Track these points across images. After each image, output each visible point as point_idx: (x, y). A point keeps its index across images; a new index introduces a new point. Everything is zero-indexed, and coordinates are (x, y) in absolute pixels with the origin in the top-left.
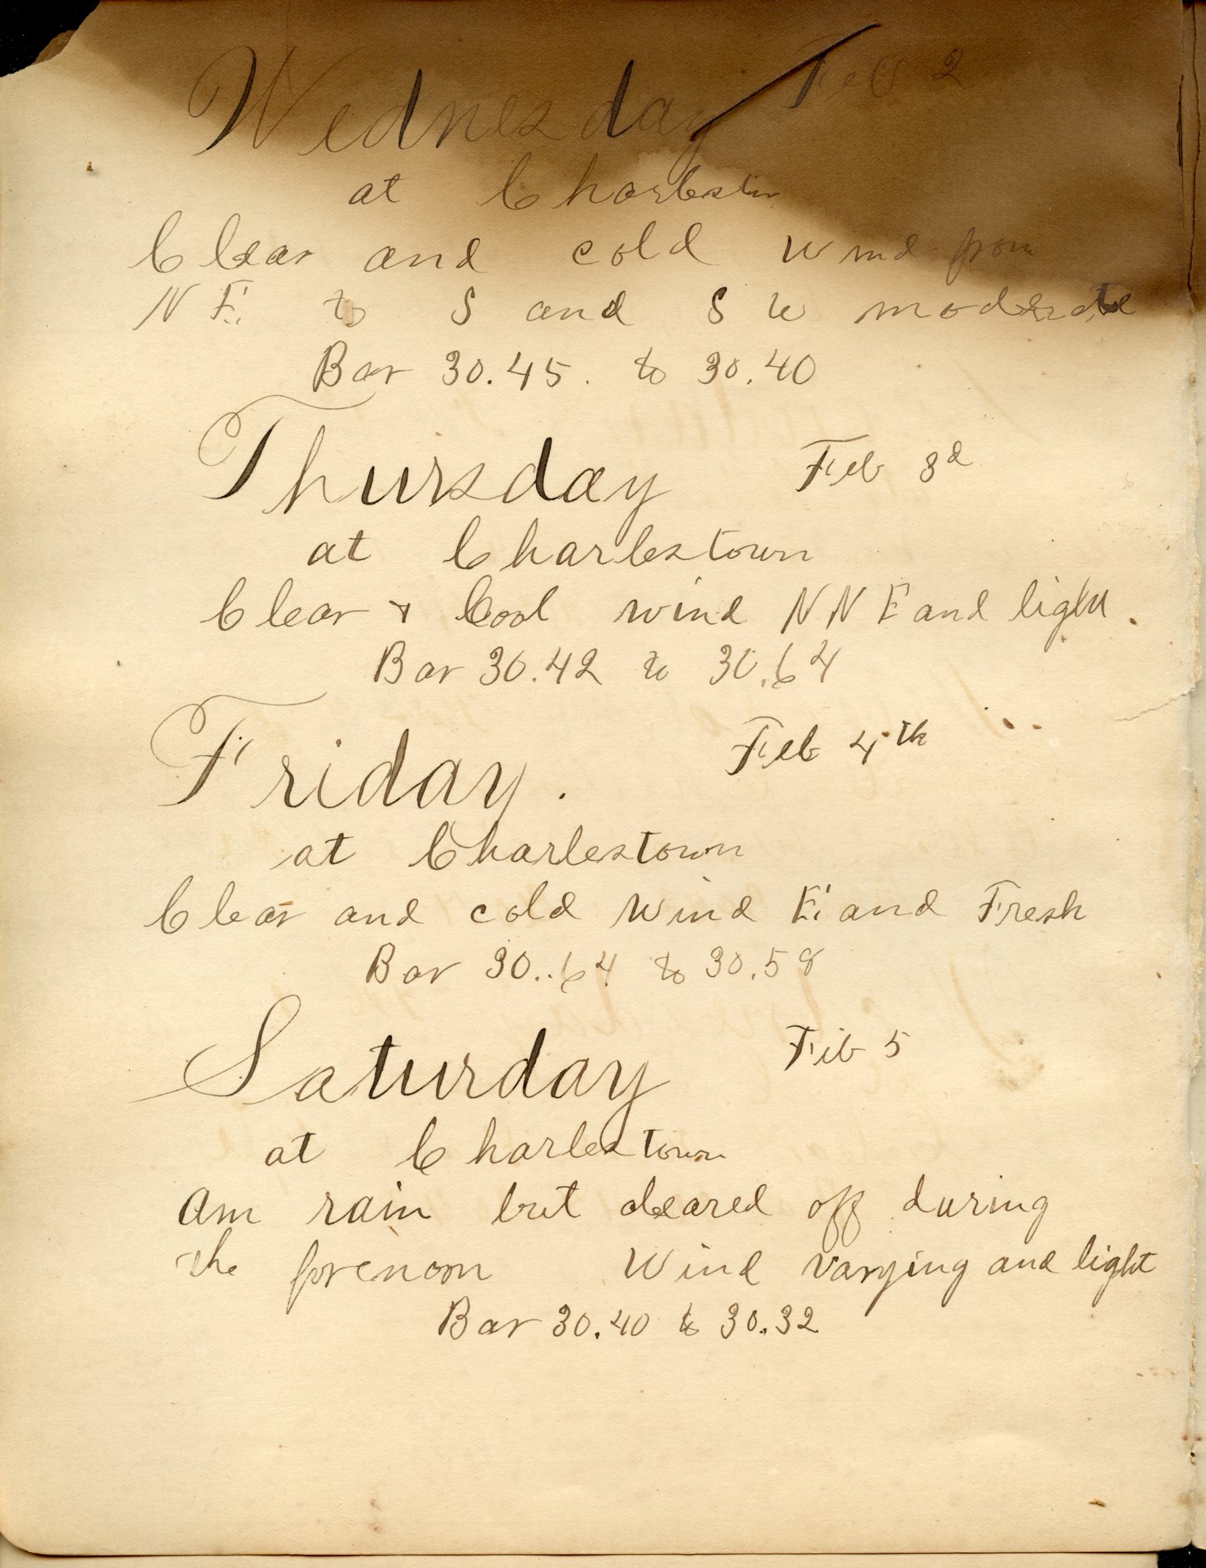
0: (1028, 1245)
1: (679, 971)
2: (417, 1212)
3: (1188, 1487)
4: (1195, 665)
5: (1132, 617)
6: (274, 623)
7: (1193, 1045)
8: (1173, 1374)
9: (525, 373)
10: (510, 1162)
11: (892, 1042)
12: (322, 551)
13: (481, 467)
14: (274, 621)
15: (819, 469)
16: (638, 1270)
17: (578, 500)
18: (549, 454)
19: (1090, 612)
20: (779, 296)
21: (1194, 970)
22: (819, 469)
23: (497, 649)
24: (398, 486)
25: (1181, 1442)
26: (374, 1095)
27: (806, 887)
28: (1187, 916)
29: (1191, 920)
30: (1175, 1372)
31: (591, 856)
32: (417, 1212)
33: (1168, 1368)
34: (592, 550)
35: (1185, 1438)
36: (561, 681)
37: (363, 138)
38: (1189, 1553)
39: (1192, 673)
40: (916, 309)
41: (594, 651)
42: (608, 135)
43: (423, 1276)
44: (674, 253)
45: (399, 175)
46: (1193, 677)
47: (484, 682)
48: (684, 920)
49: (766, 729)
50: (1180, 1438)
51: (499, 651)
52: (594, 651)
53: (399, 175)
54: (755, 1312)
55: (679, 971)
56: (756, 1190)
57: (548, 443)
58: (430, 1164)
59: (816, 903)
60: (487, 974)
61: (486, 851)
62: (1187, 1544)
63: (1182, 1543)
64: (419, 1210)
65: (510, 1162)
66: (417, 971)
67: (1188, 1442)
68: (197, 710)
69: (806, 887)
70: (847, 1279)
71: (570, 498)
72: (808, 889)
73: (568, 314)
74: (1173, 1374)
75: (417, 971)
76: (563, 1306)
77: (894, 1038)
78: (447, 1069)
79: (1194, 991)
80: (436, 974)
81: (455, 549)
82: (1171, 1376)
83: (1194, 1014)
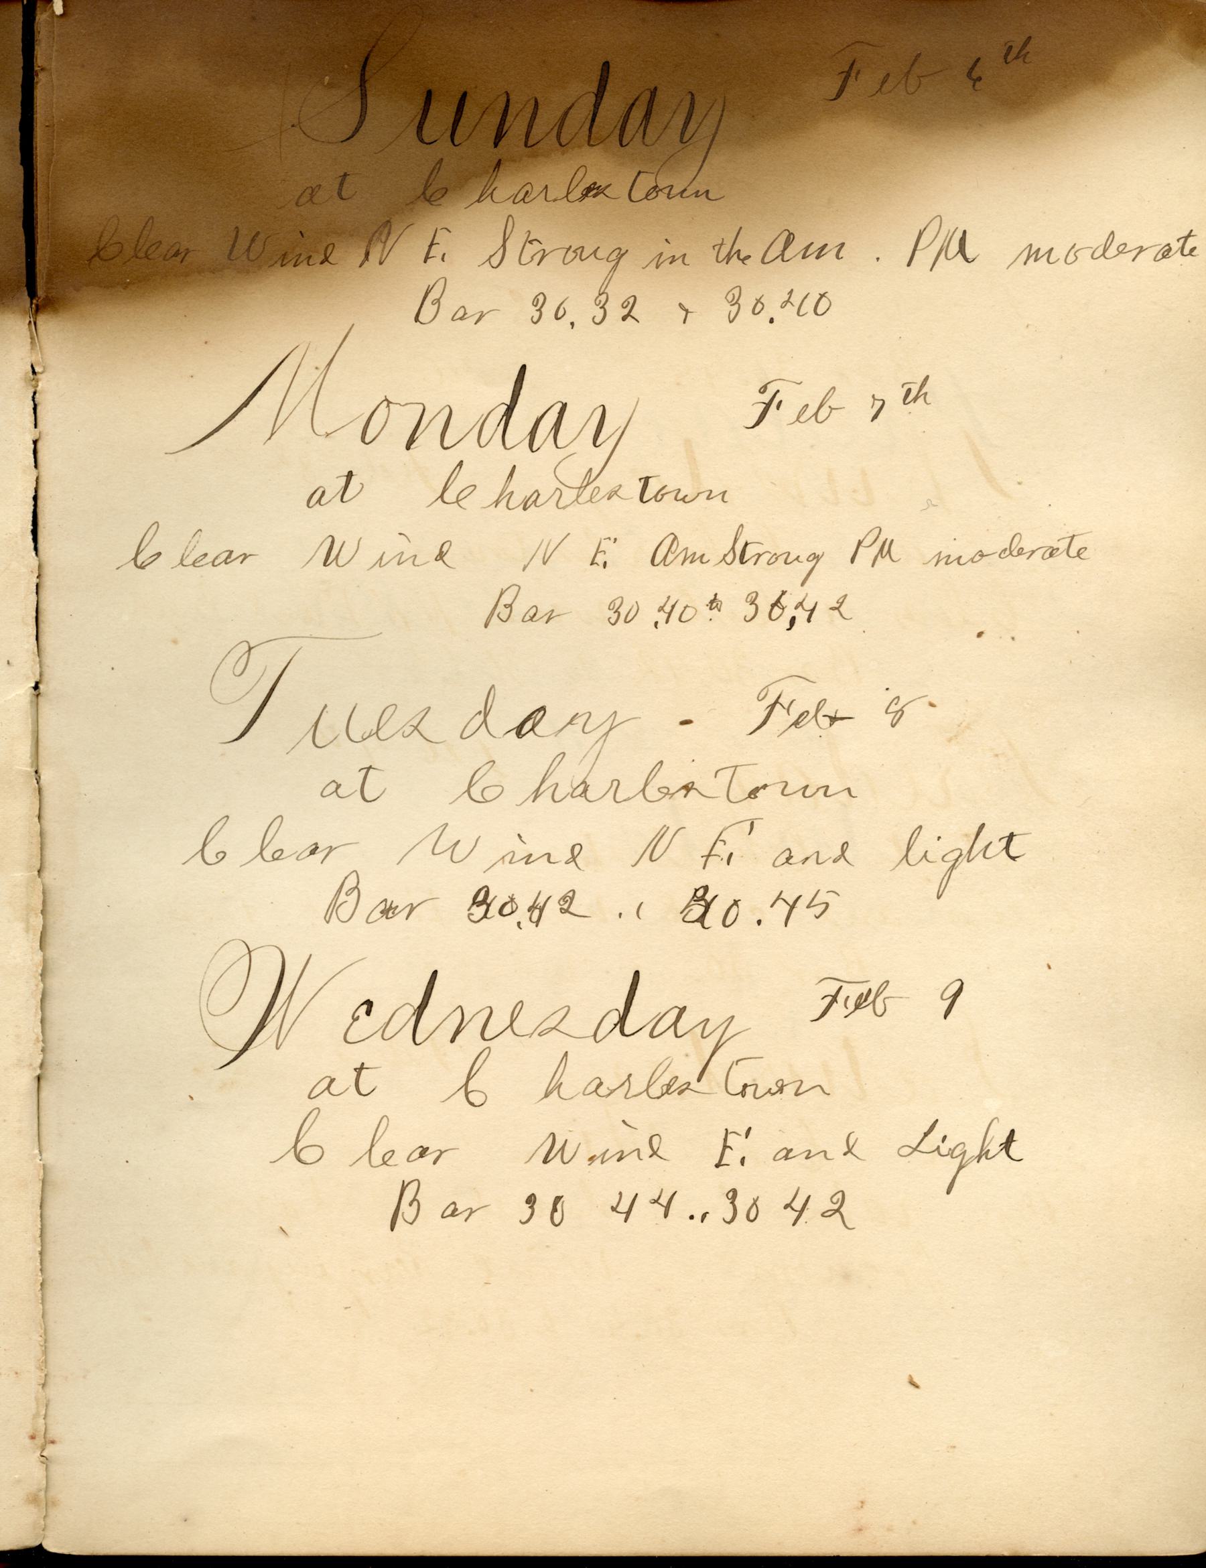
1: (363, 1064)
3: (36, 1487)
4: (33, 663)
6: (446, 499)
7: (35, 1044)
8: (17, 1373)
14: (446, 498)
15: (835, 1003)
21: (35, 970)
22: (835, 1003)
24: (414, 1018)
25: (28, 1441)
28: (27, 915)
29: (31, 920)
30: (19, 1371)
33: (11, 1368)
34: (555, 492)
35: (33, 1437)
36: (812, 619)
39: (30, 672)
46: (31, 675)
50: (27, 1437)
54: (630, 1075)
55: (363, 1064)
56: (762, 424)
61: (503, 498)
62: (37, 1543)
63: (31, 1542)
67: (36, 1441)
68: (412, 732)
74: (17, 1373)
79: (35, 991)
82: (15, 1376)
83: (35, 1013)
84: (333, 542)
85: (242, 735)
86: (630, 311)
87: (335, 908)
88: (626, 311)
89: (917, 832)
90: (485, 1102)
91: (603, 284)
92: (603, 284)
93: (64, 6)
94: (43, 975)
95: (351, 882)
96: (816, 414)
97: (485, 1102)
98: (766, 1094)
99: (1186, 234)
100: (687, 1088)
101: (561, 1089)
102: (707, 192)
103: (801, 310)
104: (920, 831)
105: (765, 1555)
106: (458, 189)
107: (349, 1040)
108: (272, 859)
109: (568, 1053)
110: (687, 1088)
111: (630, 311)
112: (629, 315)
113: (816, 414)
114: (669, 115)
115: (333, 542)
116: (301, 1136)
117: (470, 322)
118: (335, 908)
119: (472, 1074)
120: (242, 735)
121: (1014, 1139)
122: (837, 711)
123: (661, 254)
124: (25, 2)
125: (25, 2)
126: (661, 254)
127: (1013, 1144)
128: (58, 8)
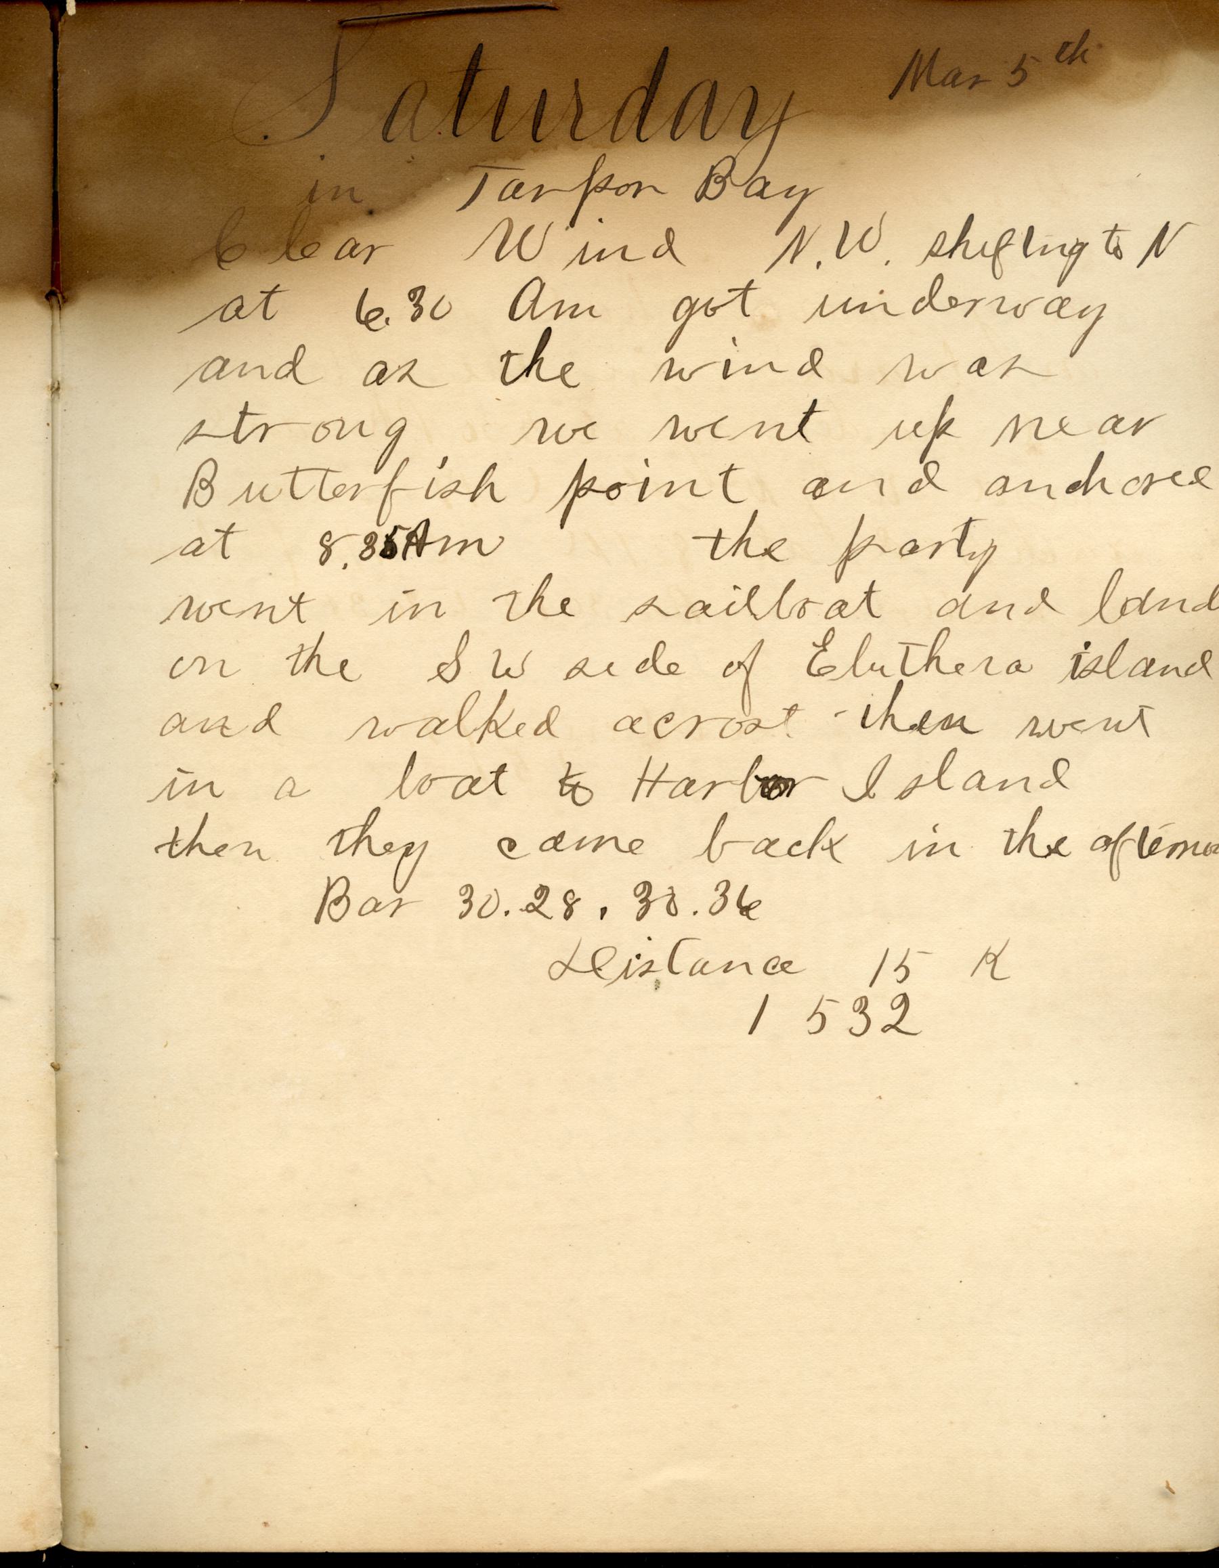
0: (1131, 678)
10: (581, 263)
11: (901, 966)
16: (457, 776)
17: (521, 319)
18: (546, 343)
19: (441, 497)
20: (993, 660)
26: (430, 496)
27: (809, 857)
37: (202, 371)
38: (646, 1559)
42: (235, 441)
45: (796, 705)
48: (434, 496)
53: (796, 705)
57: (1031, 230)
59: (934, 824)
65: (581, 263)
69: (809, 857)
71: (264, 427)
72: (806, 854)
77: (903, 962)
84: (1026, 246)
87: (442, 492)
90: (588, 802)
96: (861, 242)
97: (588, 802)
99: (727, 468)
100: (454, 490)
101: (745, 671)
103: (248, 846)
107: (749, 553)
108: (667, 672)
109: (966, 719)
110: (454, 490)
113: (861, 242)
114: (733, 102)
115: (1026, 246)
116: (657, 656)
117: (922, 556)
118: (442, 492)
121: (505, 770)
123: (245, 364)
126: (245, 364)
127: (807, 410)
128: (71, 8)
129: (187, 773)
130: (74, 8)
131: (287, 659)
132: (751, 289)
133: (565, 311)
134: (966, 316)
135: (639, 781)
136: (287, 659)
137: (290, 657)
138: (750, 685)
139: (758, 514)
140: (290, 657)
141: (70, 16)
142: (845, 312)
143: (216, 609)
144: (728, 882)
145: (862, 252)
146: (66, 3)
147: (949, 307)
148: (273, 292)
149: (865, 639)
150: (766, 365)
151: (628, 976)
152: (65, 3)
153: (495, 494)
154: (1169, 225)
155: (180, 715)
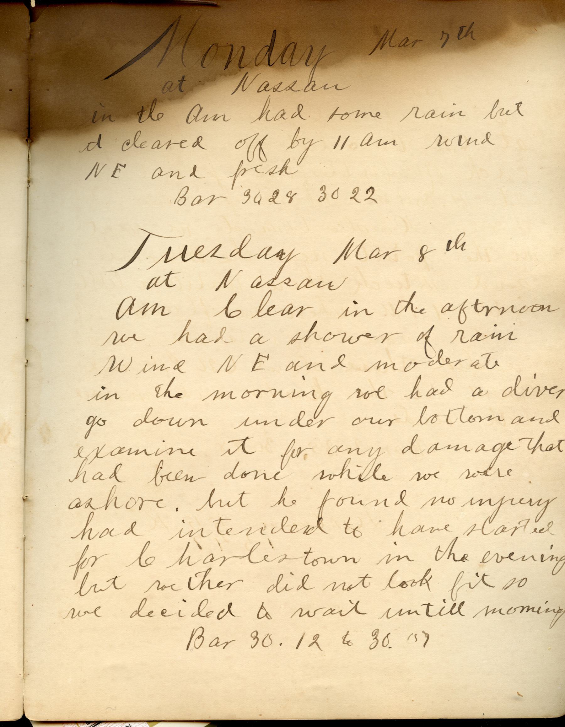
2: (144, 452)
5: (94, 177)
9: (408, 300)
12: (153, 282)
13: (90, 531)
23: (356, 188)
31: (449, 362)
32: (144, 452)
36: (448, 411)
40: (135, 501)
41: (154, 178)
43: (303, 90)
44: (233, 256)
47: (198, 647)
49: (367, 418)
51: (356, 190)
52: (154, 178)
58: (355, 586)
60: (197, 648)
64: (145, 450)
66: (284, 112)
70: (479, 388)
73: (216, 118)
75: (284, 112)
76: (523, 561)
78: (413, 390)
80: (98, 451)
81: (547, 507)
85: (124, 300)
86: (355, 196)
88: (353, 195)
89: (86, 577)
91: (301, 156)
92: (301, 156)
93: (36, 3)
94: (29, 87)
95: (199, 633)
98: (329, 613)
102: (500, 610)
104: (111, 476)
105: (418, 719)
106: (72, 129)
111: (355, 196)
112: (353, 198)
119: (279, 582)
120: (124, 300)
122: (194, 116)
124: (33, 4)
125: (33, 4)
129: (488, 451)
130: (35, 4)
131: (108, 581)
132: (367, 577)
133: (219, 395)
134: (220, 566)
135: (345, 526)
136: (108, 581)
137: (109, 581)
138: (300, 131)
139: (416, 294)
140: (109, 581)
141: (32, 8)
142: (144, 372)
143: (165, 478)
144: (337, 506)
145: (232, 400)
146: (30, 1)
147: (175, 479)
148: (365, 577)
149: (414, 437)
150: (448, 613)
151: (301, 308)
152: (30, 1)
153: (401, 533)
154: (231, 271)
155: (160, 583)
